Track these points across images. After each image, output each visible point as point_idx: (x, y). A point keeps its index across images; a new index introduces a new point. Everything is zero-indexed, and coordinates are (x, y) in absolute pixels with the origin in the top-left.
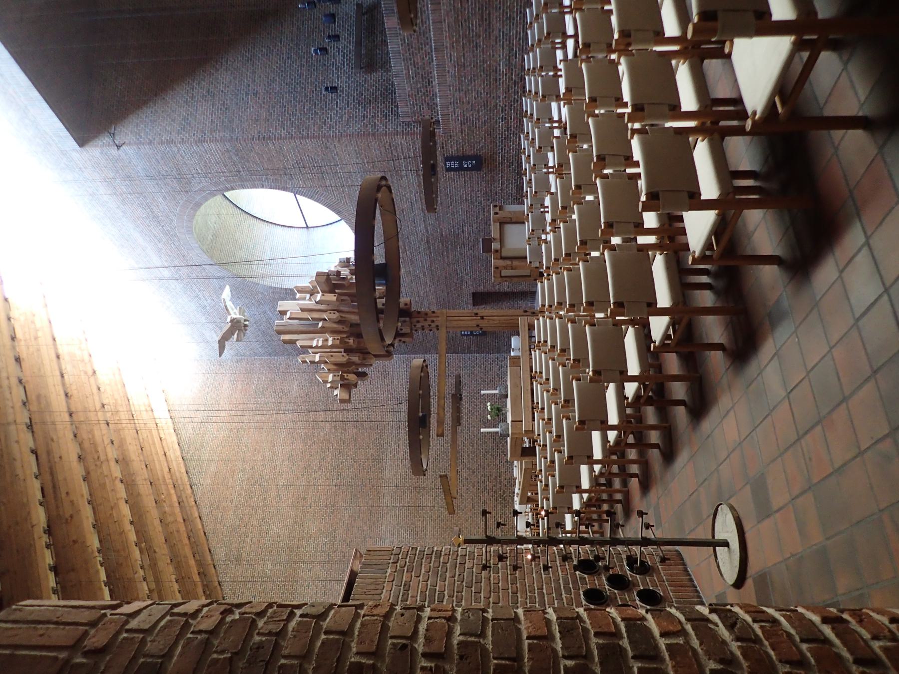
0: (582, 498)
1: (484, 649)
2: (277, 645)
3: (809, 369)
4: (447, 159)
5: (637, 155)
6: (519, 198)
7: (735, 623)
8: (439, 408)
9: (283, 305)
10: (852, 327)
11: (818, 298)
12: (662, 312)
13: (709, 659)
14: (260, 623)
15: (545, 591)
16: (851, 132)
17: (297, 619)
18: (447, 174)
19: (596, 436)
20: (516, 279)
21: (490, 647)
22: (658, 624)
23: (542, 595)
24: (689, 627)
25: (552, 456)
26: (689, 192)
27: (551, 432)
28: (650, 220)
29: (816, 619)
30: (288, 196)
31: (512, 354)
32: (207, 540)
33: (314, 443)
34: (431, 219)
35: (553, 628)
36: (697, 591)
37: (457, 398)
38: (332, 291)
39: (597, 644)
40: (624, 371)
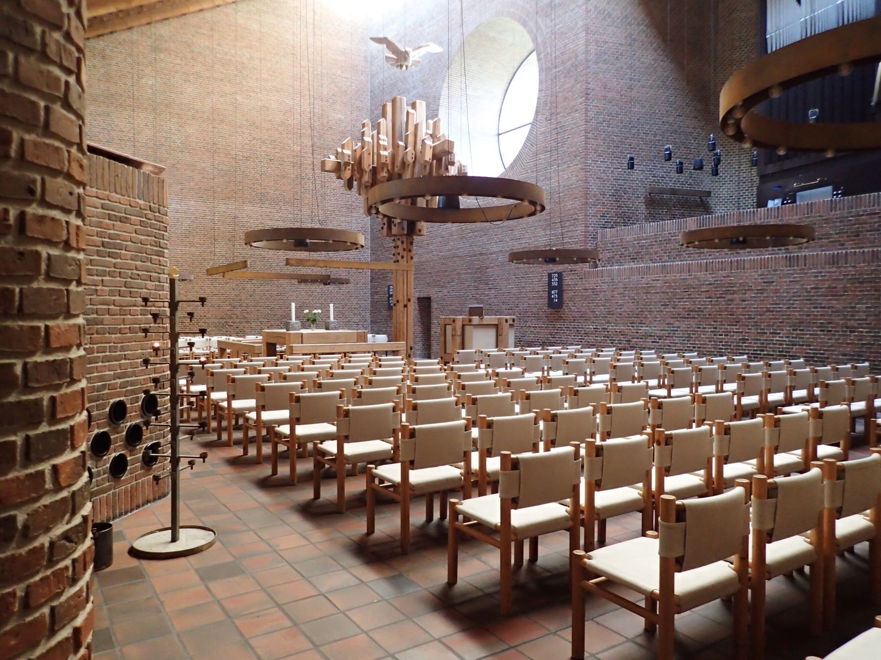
0: (223, 400)
1: (32, 279)
2: (30, 51)
3: (347, 613)
4: (560, 276)
5: (555, 451)
6: (521, 343)
7: (70, 541)
8: (314, 261)
9: (421, 105)
10: (386, 651)
11: (414, 619)
12: (405, 475)
13: (28, 514)
14: (57, 36)
15: (123, 361)
16: (570, 646)
17: (63, 77)
18: (545, 274)
19: (285, 414)
20: (442, 339)
21: (35, 285)
22: (66, 463)
23: (118, 359)
24: (65, 494)
25: (266, 372)
26: (518, 498)
27: (290, 370)
28: (494, 464)
29: (79, 622)
30: (530, 118)
31: (370, 336)
32: (177, 17)
34: (504, 258)
35: (60, 354)
36: (126, 513)
37: (326, 280)
38: (434, 156)
39: (41, 399)
40: (347, 439)
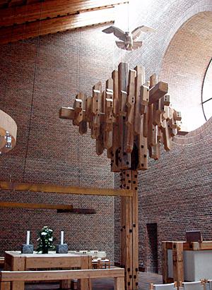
33: (54, 113)
